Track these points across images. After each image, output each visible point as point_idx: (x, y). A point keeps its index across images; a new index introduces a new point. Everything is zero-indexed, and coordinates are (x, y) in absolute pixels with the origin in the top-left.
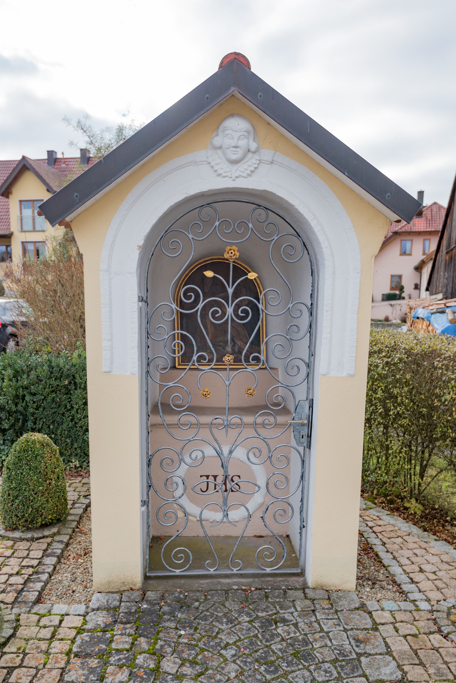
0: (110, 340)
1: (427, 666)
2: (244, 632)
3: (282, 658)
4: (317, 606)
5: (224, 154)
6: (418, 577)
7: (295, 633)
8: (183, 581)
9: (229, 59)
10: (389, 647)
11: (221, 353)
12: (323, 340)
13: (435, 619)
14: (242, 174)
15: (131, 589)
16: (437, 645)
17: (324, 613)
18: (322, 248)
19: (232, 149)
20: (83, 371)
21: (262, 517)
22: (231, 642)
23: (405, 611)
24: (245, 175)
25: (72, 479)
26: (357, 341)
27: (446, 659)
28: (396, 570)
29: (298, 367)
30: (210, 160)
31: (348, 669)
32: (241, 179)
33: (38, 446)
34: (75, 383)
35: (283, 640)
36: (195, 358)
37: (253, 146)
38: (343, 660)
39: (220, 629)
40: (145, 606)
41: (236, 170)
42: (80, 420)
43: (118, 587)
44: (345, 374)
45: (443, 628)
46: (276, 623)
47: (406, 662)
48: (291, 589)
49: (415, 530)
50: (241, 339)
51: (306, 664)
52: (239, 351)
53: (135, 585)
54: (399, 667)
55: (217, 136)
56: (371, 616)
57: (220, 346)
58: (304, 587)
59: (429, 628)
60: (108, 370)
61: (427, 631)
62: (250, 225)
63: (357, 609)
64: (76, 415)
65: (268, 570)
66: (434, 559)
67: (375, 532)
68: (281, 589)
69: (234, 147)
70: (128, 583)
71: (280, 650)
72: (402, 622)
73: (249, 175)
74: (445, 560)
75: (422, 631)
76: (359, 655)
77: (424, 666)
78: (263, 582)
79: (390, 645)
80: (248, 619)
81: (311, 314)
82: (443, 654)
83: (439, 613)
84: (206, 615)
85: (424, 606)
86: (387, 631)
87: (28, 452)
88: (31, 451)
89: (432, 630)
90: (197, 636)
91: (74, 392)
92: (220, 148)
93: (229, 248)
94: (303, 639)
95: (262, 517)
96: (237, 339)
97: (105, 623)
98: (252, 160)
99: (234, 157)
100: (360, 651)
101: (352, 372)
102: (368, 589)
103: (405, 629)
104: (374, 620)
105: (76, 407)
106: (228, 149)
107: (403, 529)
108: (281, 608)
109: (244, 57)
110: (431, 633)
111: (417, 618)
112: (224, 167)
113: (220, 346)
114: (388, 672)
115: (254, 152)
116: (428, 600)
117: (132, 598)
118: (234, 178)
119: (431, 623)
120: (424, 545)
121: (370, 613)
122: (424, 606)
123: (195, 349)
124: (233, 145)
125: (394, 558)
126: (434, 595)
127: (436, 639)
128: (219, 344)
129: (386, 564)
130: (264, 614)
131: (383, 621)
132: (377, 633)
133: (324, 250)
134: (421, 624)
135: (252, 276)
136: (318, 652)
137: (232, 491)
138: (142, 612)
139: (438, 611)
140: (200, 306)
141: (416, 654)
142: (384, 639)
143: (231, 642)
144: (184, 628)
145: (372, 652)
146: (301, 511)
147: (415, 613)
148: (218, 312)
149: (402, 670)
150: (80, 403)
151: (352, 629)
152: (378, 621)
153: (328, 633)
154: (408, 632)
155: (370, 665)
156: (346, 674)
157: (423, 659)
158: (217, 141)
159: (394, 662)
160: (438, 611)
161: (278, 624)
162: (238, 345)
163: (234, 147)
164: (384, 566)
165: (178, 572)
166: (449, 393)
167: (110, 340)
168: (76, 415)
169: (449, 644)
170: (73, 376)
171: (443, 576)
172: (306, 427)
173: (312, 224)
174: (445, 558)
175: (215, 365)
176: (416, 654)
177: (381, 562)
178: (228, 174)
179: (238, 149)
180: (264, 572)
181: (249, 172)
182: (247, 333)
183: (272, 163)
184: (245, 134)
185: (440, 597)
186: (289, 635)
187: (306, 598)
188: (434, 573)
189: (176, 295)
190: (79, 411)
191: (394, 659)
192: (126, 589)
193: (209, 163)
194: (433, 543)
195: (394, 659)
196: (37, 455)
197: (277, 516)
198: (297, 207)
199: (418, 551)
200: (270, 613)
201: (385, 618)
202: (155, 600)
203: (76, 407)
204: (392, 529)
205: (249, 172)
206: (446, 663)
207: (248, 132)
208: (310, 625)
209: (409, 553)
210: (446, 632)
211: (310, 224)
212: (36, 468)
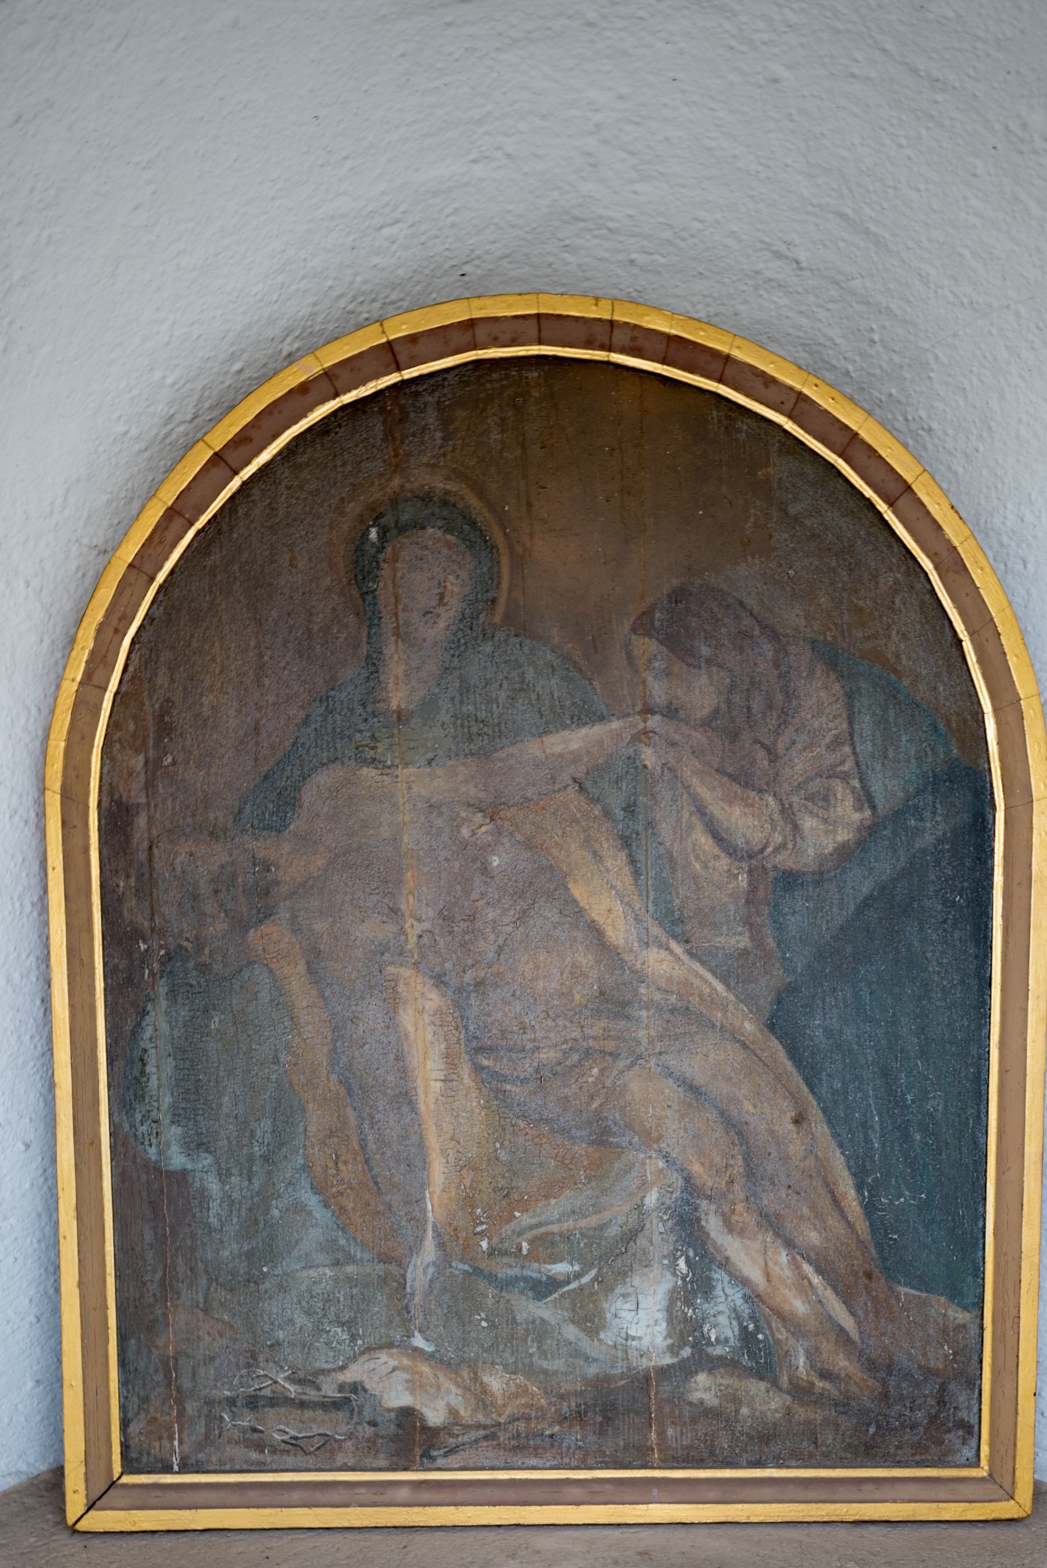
11: (558, 1364)
25: (188, 386)
50: (771, 1222)
52: (747, 1338)
57: (544, 1288)
67: (563, 1131)
96: (729, 1225)
113: (544, 1288)
128: (534, 1271)
136: (464, 1380)
162: (743, 1282)
182: (838, 1161)
189: (58, 746)
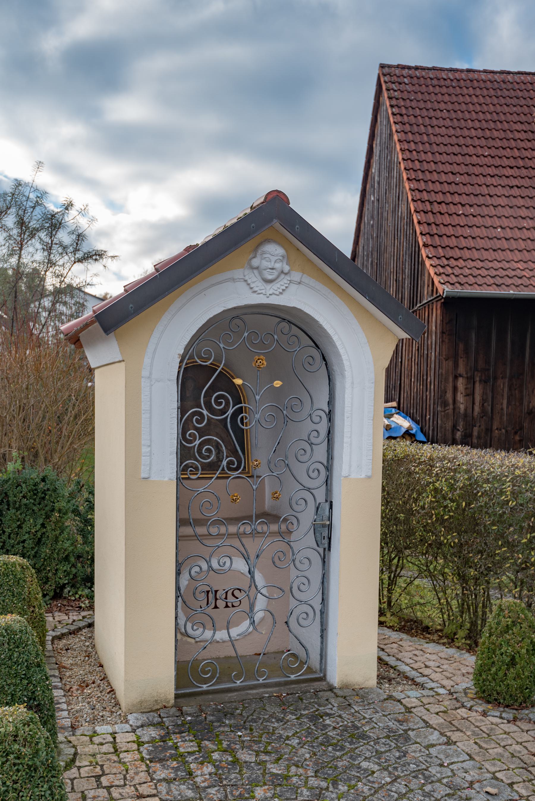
0: (150, 446)
1: (464, 730)
2: (297, 726)
3: (342, 740)
4: (350, 701)
5: (260, 273)
6: (426, 672)
7: (343, 722)
8: (210, 696)
9: (272, 196)
10: (427, 723)
12: (345, 445)
13: (456, 699)
14: (275, 292)
15: (165, 707)
16: (466, 716)
17: (360, 705)
18: (342, 360)
19: (268, 270)
20: (17, 487)
21: (286, 622)
22: (290, 735)
23: (428, 696)
24: (278, 293)
26: (373, 445)
27: (476, 724)
28: (404, 668)
29: (318, 470)
30: (246, 278)
31: (401, 740)
32: (274, 296)
33: (19, 568)
34: (8, 501)
35: (334, 728)
36: (224, 463)
37: (287, 268)
38: (394, 736)
39: (273, 727)
40: (189, 718)
41: (270, 289)
42: (13, 547)
43: (151, 706)
44: (363, 476)
45: (465, 704)
46: (322, 717)
47: (446, 730)
48: (320, 691)
49: (404, 636)
51: (366, 742)
53: (168, 702)
54: (442, 734)
55: (254, 257)
56: (401, 703)
58: (331, 689)
59: (454, 705)
60: (146, 476)
61: (453, 707)
62: (276, 337)
63: (387, 699)
64: (8, 540)
65: (293, 677)
66: (434, 657)
68: (310, 692)
69: (270, 269)
70: (161, 701)
71: (338, 735)
72: (429, 704)
73: (281, 293)
74: (443, 656)
75: (449, 708)
76: (406, 731)
77: (462, 731)
78: (290, 689)
79: (428, 720)
80: (294, 717)
81: (330, 421)
82: (473, 721)
83: (458, 694)
84: (253, 719)
85: (441, 691)
86: (420, 711)
87: (8, 576)
88: (12, 574)
89: (457, 706)
90: (255, 734)
91: (7, 513)
92: (257, 268)
93: (257, 357)
94: (353, 726)
95: (286, 622)
97: (159, 735)
98: (284, 281)
99: (270, 277)
100: (404, 728)
101: (370, 474)
102: (387, 686)
103: (435, 708)
104: (404, 706)
105: (8, 530)
106: (265, 270)
107: (393, 637)
108: (320, 705)
109: (277, 191)
110: (456, 709)
111: (441, 700)
112: (259, 285)
114: (435, 738)
115: (286, 274)
116: (444, 687)
117: (171, 713)
118: (268, 295)
119: (454, 702)
120: (420, 648)
121: (399, 701)
122: (441, 691)
123: (225, 454)
124: (270, 267)
125: (398, 659)
126: (447, 683)
127: (463, 712)
129: (393, 665)
130: (306, 712)
131: (413, 705)
132: (412, 714)
133: (345, 362)
134: (446, 703)
135: (277, 384)
137: (233, 606)
138: (190, 723)
139: (456, 693)
140: (230, 411)
141: (451, 724)
142: (420, 718)
143: (290, 735)
144: (240, 730)
145: (415, 727)
146: (322, 613)
147: (437, 697)
148: (197, 419)
149: (446, 736)
150: (14, 525)
151: (389, 714)
152: (409, 706)
153: (371, 719)
154: (438, 710)
155: (417, 736)
156: (401, 743)
157: (459, 727)
158: (255, 262)
159: (436, 731)
160: (456, 693)
161: (324, 717)
163: (270, 269)
164: (392, 667)
165: (205, 687)
166: (428, 497)
167: (150, 446)
168: (8, 540)
169: (474, 714)
170: (6, 493)
171: (447, 668)
172: (327, 529)
173: (334, 339)
174: (443, 655)
175: (201, 474)
176: (451, 724)
177: (387, 664)
178: (263, 291)
179: (274, 271)
180: (289, 679)
181: (281, 291)
183: (300, 283)
184: (281, 258)
185: (452, 683)
186: (338, 724)
187: (337, 696)
188: (438, 667)
190: (12, 536)
191: (435, 729)
192: (159, 707)
193: (246, 281)
194: (426, 645)
195: (435, 729)
196: (20, 579)
197: (301, 621)
198: (321, 323)
199: (416, 652)
200: (312, 710)
201: (414, 702)
202: (195, 713)
203: (8, 530)
204: (384, 637)
205: (281, 291)
206: (477, 727)
207: (283, 257)
208: (353, 715)
209: (410, 655)
210: (469, 706)
211: (332, 339)
212: (20, 594)
